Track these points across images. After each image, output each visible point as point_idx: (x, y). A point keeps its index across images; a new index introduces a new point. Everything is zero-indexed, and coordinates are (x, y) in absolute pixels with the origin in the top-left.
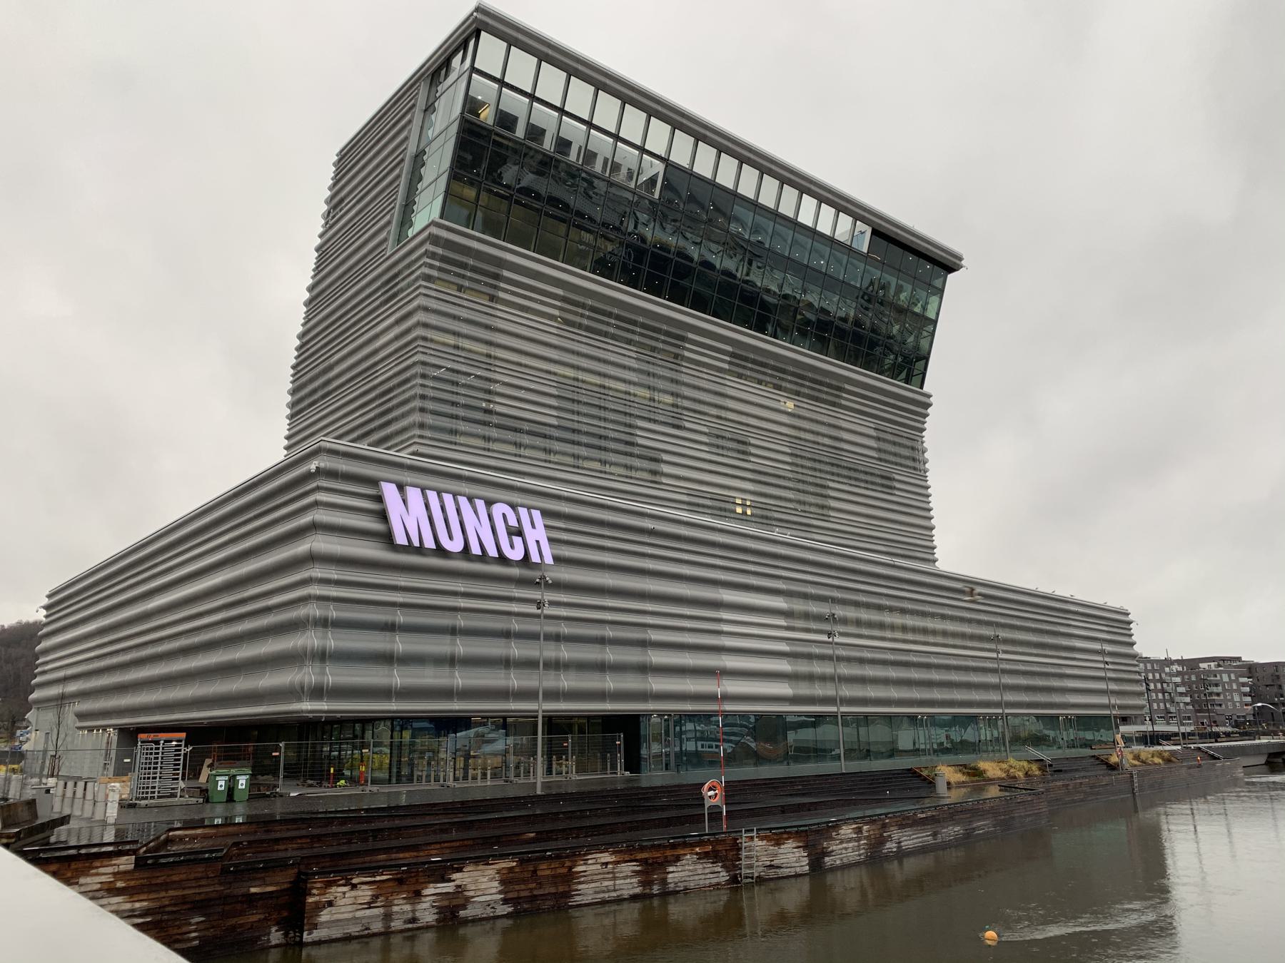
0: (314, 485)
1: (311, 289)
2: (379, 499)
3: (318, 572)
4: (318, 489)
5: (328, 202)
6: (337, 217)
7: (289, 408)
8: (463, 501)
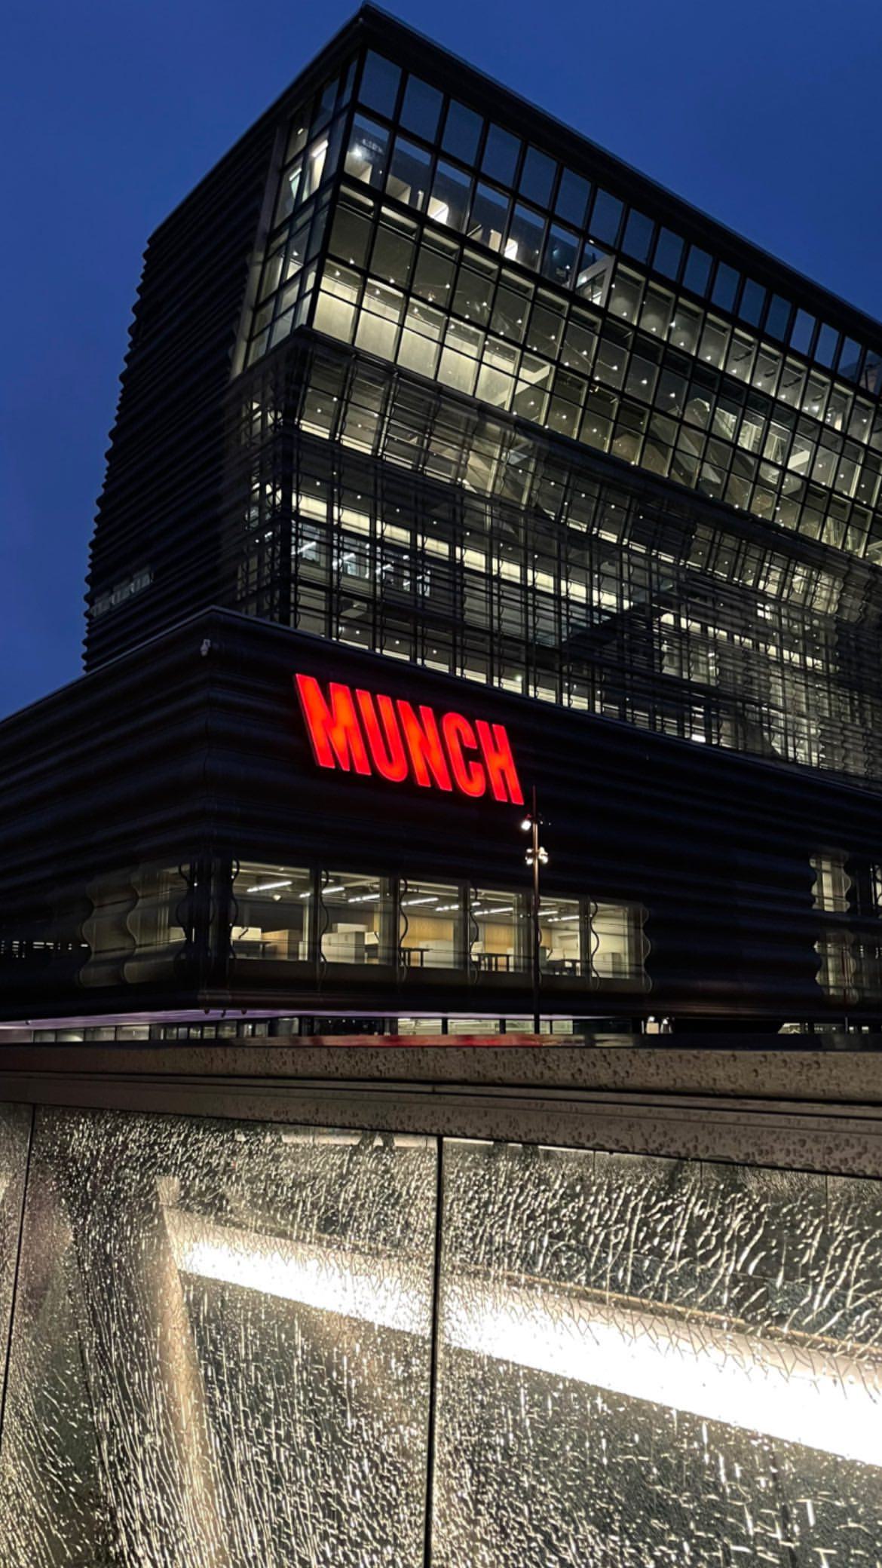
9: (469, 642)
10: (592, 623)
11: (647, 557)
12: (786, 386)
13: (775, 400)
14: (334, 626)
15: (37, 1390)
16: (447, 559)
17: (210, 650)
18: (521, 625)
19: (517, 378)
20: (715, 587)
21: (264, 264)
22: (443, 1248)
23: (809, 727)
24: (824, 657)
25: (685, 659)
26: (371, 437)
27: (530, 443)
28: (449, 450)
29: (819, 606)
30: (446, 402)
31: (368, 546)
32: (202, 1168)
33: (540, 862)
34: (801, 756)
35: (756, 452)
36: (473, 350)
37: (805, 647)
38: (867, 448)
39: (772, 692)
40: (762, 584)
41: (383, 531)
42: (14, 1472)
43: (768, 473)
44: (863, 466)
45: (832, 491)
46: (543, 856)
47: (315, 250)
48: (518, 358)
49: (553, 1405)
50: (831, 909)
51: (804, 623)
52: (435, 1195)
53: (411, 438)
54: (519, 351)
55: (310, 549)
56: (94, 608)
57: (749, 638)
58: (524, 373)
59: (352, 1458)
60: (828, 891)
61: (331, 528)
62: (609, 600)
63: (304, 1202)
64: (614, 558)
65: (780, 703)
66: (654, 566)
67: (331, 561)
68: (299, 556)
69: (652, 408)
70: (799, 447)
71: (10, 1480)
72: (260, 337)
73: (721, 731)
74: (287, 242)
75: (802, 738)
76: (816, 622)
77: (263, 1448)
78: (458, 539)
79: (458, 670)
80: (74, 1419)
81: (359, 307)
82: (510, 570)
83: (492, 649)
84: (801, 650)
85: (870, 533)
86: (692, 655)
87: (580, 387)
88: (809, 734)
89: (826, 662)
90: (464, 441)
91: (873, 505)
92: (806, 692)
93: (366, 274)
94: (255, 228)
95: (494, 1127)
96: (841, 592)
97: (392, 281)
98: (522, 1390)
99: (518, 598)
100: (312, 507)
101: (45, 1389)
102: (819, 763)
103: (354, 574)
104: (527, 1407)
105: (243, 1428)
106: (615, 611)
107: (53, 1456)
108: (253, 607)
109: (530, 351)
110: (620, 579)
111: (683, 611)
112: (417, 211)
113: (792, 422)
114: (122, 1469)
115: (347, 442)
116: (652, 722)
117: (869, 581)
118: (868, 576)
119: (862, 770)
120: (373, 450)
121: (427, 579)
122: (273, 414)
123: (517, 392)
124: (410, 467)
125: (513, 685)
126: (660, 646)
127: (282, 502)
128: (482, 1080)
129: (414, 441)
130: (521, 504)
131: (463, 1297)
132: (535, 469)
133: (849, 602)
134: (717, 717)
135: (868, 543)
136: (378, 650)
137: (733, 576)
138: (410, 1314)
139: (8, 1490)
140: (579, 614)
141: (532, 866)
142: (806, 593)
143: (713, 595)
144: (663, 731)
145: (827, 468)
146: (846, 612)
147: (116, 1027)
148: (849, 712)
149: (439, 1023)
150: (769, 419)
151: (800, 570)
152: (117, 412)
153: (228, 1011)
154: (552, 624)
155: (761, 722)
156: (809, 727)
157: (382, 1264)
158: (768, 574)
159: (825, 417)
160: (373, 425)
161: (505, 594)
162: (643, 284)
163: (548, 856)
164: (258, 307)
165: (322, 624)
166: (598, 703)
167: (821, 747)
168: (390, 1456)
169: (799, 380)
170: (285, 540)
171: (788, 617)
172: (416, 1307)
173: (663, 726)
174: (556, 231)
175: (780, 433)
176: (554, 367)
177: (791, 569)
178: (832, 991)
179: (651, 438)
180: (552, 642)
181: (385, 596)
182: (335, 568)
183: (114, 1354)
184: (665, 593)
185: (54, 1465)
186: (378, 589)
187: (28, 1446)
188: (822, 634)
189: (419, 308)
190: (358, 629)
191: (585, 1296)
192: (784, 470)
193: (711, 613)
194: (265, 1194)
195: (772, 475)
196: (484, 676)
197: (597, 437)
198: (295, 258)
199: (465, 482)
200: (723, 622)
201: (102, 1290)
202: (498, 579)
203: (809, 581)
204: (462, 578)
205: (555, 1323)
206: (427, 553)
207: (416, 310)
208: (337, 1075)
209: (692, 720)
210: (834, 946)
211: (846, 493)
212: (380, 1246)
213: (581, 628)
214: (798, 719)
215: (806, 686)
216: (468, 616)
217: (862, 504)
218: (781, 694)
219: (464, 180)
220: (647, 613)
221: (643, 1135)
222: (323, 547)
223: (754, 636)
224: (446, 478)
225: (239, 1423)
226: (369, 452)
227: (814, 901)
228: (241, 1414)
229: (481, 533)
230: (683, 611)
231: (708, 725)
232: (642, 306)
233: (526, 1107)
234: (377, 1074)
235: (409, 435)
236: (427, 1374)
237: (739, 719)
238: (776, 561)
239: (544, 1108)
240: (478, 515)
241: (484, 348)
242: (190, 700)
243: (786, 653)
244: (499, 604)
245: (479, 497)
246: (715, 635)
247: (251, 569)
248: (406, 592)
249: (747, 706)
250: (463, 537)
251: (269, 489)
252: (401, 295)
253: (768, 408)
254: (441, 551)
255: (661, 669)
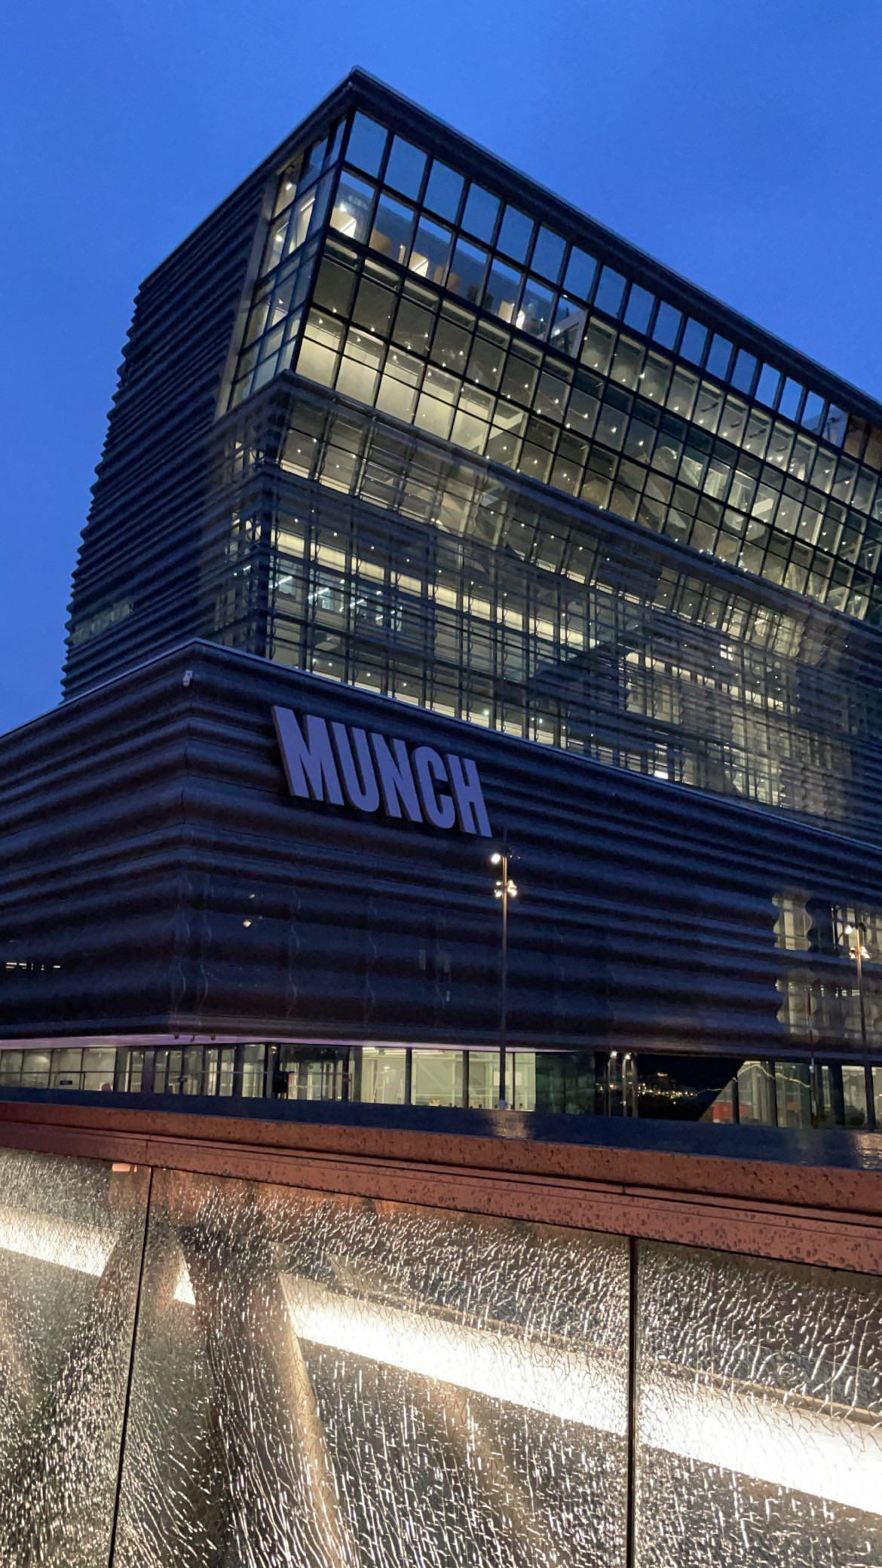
0: (187, 705)
1: (100, 470)
2: (270, 731)
3: (189, 830)
4: (192, 712)
5: (126, 351)
6: (138, 374)
7: (68, 629)
8: (378, 740)
9: (439, 677)
10: (559, 660)
11: (614, 597)
12: (751, 437)
13: (740, 450)
14: (308, 658)
15: (160, 1454)
16: (419, 595)
17: (192, 681)
18: (490, 661)
19: (491, 424)
20: (679, 628)
21: (251, 310)
22: (639, 1348)
23: (770, 766)
24: (785, 699)
25: (649, 697)
26: (349, 477)
27: (502, 487)
28: (424, 491)
29: (781, 648)
30: (422, 446)
31: (343, 581)
32: (352, 1245)
33: (508, 895)
34: (762, 795)
35: (720, 499)
36: (449, 397)
37: (766, 689)
38: (829, 497)
39: (733, 731)
40: (725, 626)
41: (357, 567)
42: (135, 1534)
43: (732, 519)
44: (825, 515)
45: (794, 538)
46: (512, 889)
47: (300, 299)
48: (492, 405)
49: (772, 1511)
50: (792, 948)
51: (765, 665)
52: (628, 1294)
53: (387, 479)
54: (493, 398)
55: (286, 584)
56: (74, 635)
57: (712, 678)
58: (499, 420)
59: (538, 1546)
60: (789, 930)
61: (308, 564)
62: (575, 638)
63: (474, 1288)
64: (581, 598)
65: (742, 743)
66: (620, 607)
67: (308, 595)
68: (275, 590)
69: (621, 455)
70: (763, 495)
71: (130, 1541)
72: (244, 381)
73: (684, 769)
74: (273, 292)
75: (763, 777)
76: (777, 665)
77: (432, 1530)
78: (431, 578)
79: (428, 703)
80: (205, 1485)
81: (340, 353)
82: (480, 608)
83: (461, 684)
84: (763, 691)
85: (831, 579)
86: (656, 694)
87: (552, 434)
88: (769, 773)
89: (788, 703)
90: (438, 483)
91: (835, 553)
92: (768, 732)
93: (348, 322)
94: (242, 277)
95: (698, 1233)
96: (804, 634)
97: (373, 330)
98: (735, 1494)
99: (488, 635)
100: (290, 543)
101: (170, 1452)
102: (779, 802)
103: (328, 608)
104: (741, 1510)
105: (409, 1508)
106: (581, 649)
107: (180, 1520)
108: (230, 637)
109: (504, 398)
110: (587, 618)
111: (648, 651)
112: (399, 265)
113: (757, 470)
114: (265, 1539)
115: (326, 482)
116: (617, 759)
117: (829, 626)
118: (829, 621)
119: (821, 810)
120: (350, 490)
121: (399, 615)
122: (255, 454)
123: (491, 437)
124: (385, 507)
125: (481, 719)
126: (625, 684)
127: (261, 537)
128: (682, 1186)
129: (390, 482)
130: (491, 544)
131: (663, 1397)
132: (507, 511)
133: (810, 645)
134: (680, 754)
135: (829, 588)
136: (350, 683)
137: (697, 619)
138: (603, 1410)
139: (127, 1551)
140: (546, 650)
141: (501, 899)
142: (768, 636)
143: (678, 637)
144: (626, 767)
145: (789, 517)
146: (807, 655)
147: (84, 1049)
148: (809, 753)
149: (404, 1052)
150: (734, 468)
151: (762, 613)
152: (104, 449)
153: (197, 1037)
154: (520, 660)
155: (723, 760)
156: (770, 766)
157: (566, 1356)
158: (731, 616)
159: (789, 467)
160: (351, 467)
161: (476, 631)
162: (615, 338)
163: (518, 889)
164: (243, 352)
165: (296, 656)
166: (563, 739)
167: (782, 786)
168: (583, 1547)
169: (763, 431)
170: (264, 573)
171: (750, 659)
172: (610, 1403)
173: (627, 762)
174: (532, 286)
175: (744, 482)
176: (527, 414)
177: (754, 612)
178: (793, 1030)
179: (619, 483)
180: (519, 678)
181: (359, 630)
182: (311, 602)
183: (253, 1425)
184: (630, 633)
185: (184, 1530)
186: (352, 623)
187: (152, 1509)
188: (784, 675)
189: (398, 355)
190: (331, 661)
191: (807, 1405)
192: (748, 516)
193: (674, 652)
194: (427, 1277)
195: (736, 521)
196: (453, 709)
197: (565, 480)
198: (281, 306)
199: (438, 522)
200: (687, 662)
201: (237, 1358)
202: (468, 616)
203: (771, 623)
204: (433, 614)
205: (771, 1431)
206: (401, 589)
207: (395, 357)
208: (512, 1167)
209: (655, 757)
210: (795, 985)
211: (808, 540)
212: (564, 1338)
213: (548, 664)
214: (759, 758)
215: (768, 726)
216: (438, 651)
217: (823, 551)
218: (742, 733)
219: (445, 236)
220: (612, 653)
221: (872, 1256)
222: (300, 582)
223: (717, 676)
224: (420, 518)
225: (404, 1503)
226: (347, 492)
227: (775, 941)
228: (406, 1495)
229: (452, 571)
230: (648, 651)
231: (671, 762)
232: (613, 359)
233: (735, 1217)
234: (559, 1171)
235: (386, 476)
236: (624, 1470)
237: (702, 756)
238: (739, 605)
239: (755, 1220)
240: (449, 554)
241: (460, 395)
242: (171, 729)
243: (748, 694)
244: (469, 640)
245: (452, 536)
246: (704, 683)
247: (229, 602)
248: (378, 627)
249: (710, 745)
250: (435, 575)
251: (248, 525)
252: (381, 343)
253: (735, 457)
254: (413, 588)
255: (626, 706)
